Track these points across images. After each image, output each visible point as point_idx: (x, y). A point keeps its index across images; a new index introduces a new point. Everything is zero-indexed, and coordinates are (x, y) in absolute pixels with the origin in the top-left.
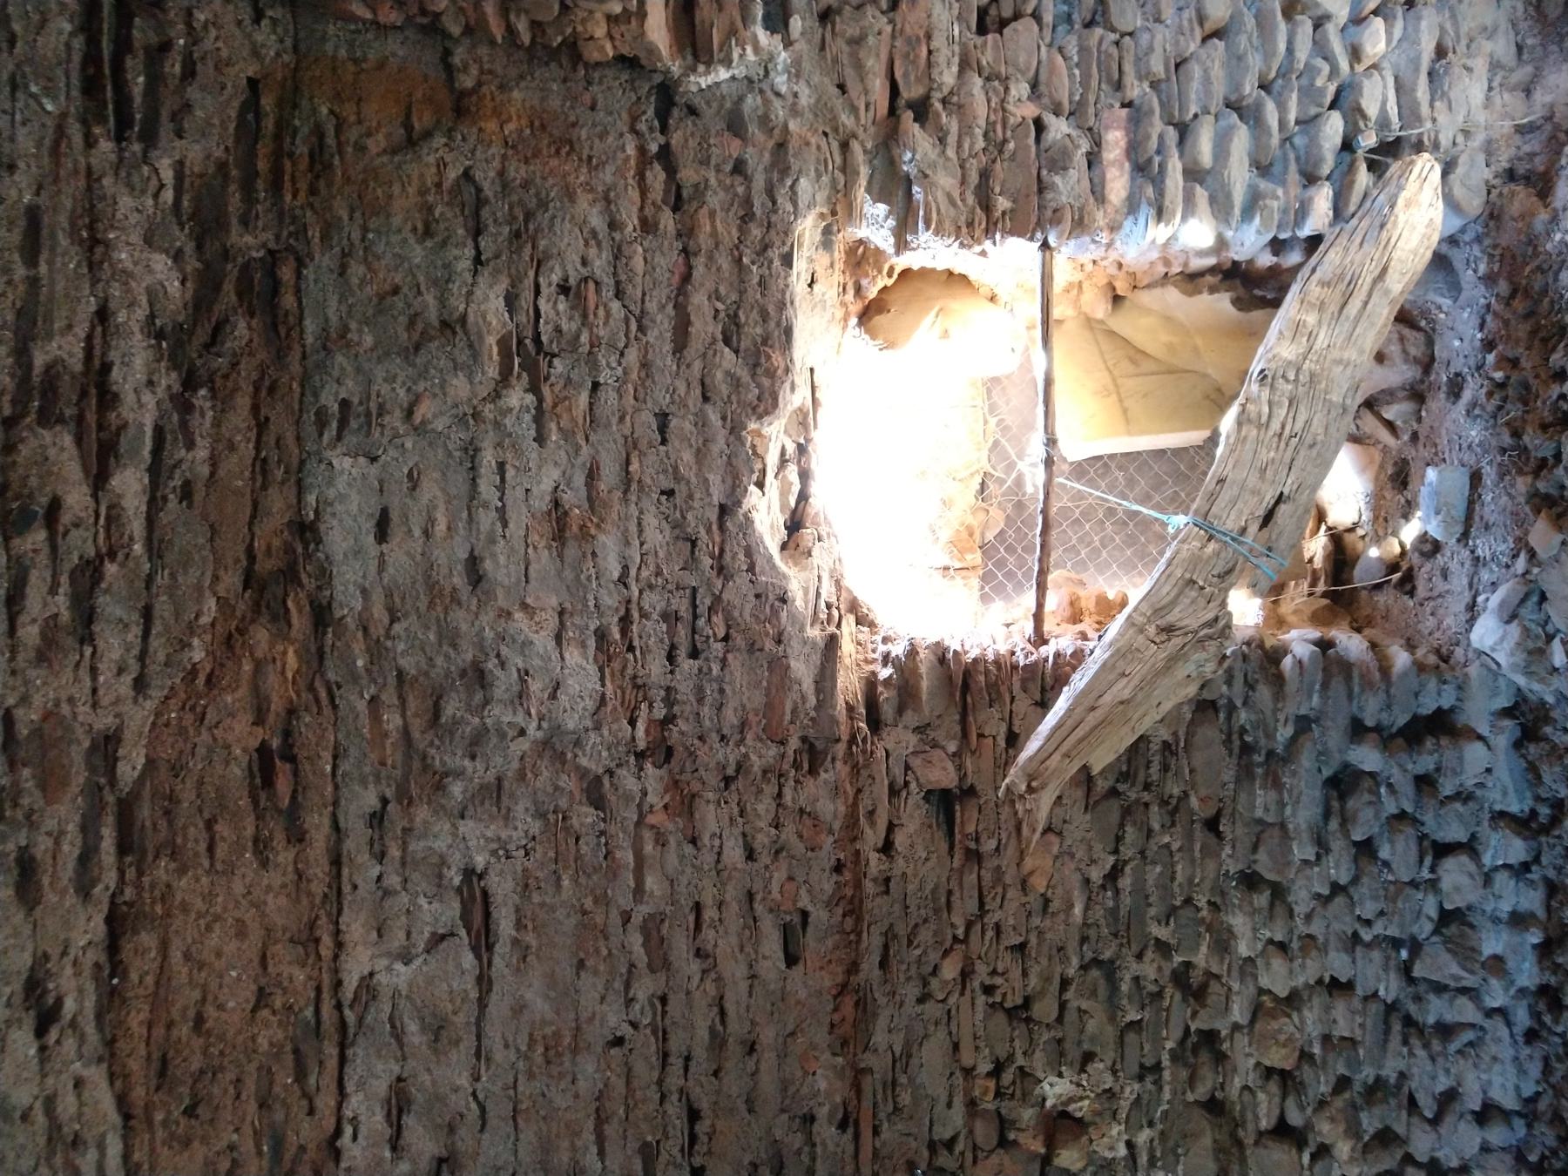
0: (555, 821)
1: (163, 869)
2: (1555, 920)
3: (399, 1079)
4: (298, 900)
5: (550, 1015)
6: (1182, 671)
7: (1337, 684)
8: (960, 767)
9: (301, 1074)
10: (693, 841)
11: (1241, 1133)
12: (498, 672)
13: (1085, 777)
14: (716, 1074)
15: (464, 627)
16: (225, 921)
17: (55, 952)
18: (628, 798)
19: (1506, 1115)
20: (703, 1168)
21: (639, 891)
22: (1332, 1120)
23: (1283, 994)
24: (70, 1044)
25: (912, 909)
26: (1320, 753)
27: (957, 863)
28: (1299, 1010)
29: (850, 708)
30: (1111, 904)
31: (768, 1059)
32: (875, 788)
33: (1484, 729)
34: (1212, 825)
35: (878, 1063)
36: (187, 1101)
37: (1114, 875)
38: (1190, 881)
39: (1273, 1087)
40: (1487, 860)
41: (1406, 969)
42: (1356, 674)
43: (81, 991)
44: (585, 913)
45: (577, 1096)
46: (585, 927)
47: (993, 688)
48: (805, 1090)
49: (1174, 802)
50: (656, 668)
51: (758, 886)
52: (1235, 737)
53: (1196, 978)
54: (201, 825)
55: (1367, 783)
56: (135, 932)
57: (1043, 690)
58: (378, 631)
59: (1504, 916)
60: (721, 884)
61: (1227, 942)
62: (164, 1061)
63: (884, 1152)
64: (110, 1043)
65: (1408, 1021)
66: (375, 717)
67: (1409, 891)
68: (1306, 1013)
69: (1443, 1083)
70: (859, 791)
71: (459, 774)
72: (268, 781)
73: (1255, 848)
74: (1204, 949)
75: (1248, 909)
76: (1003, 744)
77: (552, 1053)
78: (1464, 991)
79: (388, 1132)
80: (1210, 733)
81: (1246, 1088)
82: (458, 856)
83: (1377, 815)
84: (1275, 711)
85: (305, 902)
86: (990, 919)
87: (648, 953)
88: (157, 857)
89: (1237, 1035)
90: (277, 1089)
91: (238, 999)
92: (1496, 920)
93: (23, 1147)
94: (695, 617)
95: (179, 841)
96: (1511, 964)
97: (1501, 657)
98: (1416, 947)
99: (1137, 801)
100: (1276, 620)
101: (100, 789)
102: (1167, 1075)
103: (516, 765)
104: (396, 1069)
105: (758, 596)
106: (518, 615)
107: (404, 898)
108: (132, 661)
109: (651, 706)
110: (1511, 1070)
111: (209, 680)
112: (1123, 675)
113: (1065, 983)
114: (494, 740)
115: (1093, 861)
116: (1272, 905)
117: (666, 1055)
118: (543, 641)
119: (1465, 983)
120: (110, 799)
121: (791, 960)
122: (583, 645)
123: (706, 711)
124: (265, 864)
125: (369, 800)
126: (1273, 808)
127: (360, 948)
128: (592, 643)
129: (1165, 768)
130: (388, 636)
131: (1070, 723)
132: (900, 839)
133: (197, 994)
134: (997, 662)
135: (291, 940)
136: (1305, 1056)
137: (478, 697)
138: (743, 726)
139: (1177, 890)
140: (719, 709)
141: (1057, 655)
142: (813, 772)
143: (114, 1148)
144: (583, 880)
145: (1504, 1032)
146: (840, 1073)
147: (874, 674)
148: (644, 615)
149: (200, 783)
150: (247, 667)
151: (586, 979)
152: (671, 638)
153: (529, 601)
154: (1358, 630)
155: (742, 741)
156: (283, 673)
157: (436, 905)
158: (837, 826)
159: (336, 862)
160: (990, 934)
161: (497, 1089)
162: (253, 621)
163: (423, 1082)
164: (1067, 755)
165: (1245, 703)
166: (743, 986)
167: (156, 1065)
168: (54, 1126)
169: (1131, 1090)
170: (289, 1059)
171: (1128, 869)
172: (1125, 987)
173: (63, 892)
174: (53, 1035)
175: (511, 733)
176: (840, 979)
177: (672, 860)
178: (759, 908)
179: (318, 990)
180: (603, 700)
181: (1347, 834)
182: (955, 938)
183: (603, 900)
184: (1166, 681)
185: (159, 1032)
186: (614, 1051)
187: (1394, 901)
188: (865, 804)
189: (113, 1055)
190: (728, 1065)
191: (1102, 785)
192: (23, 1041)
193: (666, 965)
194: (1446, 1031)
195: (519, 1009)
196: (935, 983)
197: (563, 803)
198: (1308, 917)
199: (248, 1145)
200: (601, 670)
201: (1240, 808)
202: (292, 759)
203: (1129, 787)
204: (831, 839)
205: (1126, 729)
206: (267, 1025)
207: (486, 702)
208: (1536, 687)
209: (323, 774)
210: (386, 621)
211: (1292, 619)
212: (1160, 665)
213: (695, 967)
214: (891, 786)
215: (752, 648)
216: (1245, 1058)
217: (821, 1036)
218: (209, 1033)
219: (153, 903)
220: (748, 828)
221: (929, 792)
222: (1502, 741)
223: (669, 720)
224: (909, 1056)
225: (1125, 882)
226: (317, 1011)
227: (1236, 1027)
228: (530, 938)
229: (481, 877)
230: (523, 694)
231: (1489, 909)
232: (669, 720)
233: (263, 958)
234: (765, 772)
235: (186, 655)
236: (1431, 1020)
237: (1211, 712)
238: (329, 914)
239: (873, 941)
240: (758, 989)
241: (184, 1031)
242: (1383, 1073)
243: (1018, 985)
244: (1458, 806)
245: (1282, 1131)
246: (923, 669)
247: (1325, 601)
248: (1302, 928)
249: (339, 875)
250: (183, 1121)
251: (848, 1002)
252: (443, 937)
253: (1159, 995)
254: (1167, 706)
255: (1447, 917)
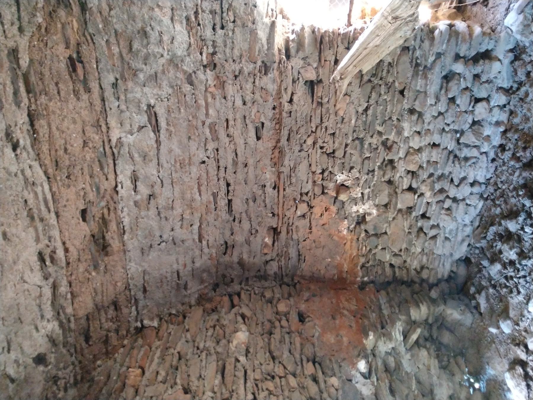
0: (177, 89)
1: (43, 99)
2: (510, 123)
3: (134, 171)
4: (92, 112)
5: (181, 154)
6: (398, 35)
7: (453, 40)
8: (317, 72)
9: (102, 168)
10: (225, 98)
11: (397, 190)
12: (151, 32)
13: (360, 75)
14: (235, 173)
15: (137, 13)
16: (69, 117)
17: (13, 125)
18: (201, 82)
19: (480, 184)
20: (231, 200)
21: (207, 114)
22: (426, 186)
23: (417, 148)
24: (25, 154)
25: (298, 122)
26: (443, 66)
27: (314, 106)
28: (421, 153)
29: (280, 50)
30: (364, 119)
31: (251, 169)
32: (287, 80)
33: (501, 57)
34: (402, 92)
35: (285, 170)
36: (66, 175)
37: (366, 110)
38: (392, 112)
39: (409, 176)
40: (492, 104)
41: (458, 140)
42: (460, 37)
43: (24, 138)
44: (189, 121)
45: (191, 178)
46: (189, 125)
47: (331, 42)
48: (263, 178)
49: (390, 84)
50: (208, 32)
51: (247, 114)
52: (414, 60)
53: (389, 143)
54: (54, 84)
55: (457, 77)
56: (38, 120)
57: (349, 43)
58: (105, 14)
59: (493, 122)
60: (235, 113)
61: (401, 132)
62: (57, 162)
63: (287, 196)
64: (38, 155)
65: (456, 156)
66: (109, 48)
67: (464, 114)
68: (423, 154)
69: (462, 175)
70: (282, 81)
71: (142, 70)
72: (75, 70)
73: (415, 100)
74: (393, 134)
75: (409, 120)
76: (333, 63)
77: (182, 165)
78: (475, 146)
79: (132, 186)
80: (406, 59)
81: (401, 177)
82: (144, 99)
83: (458, 88)
84: (429, 51)
85: (94, 113)
86: (324, 125)
87: (211, 135)
88: (40, 94)
89: (400, 161)
90: (95, 172)
91: (77, 144)
92: (490, 124)
93: (17, 184)
94: (222, 12)
95: (47, 89)
96: (492, 138)
97: (514, 29)
98: (462, 133)
99: (377, 84)
100: (436, 19)
101: (15, 69)
102: (376, 173)
103: (161, 68)
104: (133, 168)
105: (245, 4)
106: (156, 10)
107: (128, 114)
108: (16, 20)
109: (207, 48)
110: (485, 170)
111: (46, 29)
112: (378, 36)
113: (347, 145)
114: (152, 58)
115: (360, 105)
116: (418, 119)
117: (219, 167)
118: (166, 20)
119: (476, 144)
120: (20, 73)
121: (258, 138)
122: (181, 23)
123: (228, 51)
124: (78, 99)
125: (111, 79)
126: (423, 86)
127: (115, 129)
128: (184, 22)
129: (388, 72)
130: (109, 16)
131: (357, 54)
132: (295, 98)
133: (63, 142)
134: (333, 32)
135: (92, 125)
136: (421, 167)
137: (145, 42)
138: (241, 56)
139: (387, 114)
140: (232, 50)
141: (355, 29)
142: (266, 74)
143: (46, 187)
144: (188, 110)
145: (485, 159)
146: (274, 173)
147: (288, 37)
148: (203, 11)
149: (50, 69)
150: (59, 26)
151: (192, 143)
152: (214, 21)
153: (160, 4)
154: (465, 21)
155: (241, 61)
156: (73, 29)
157: (139, 116)
158: (274, 93)
159: (103, 100)
160: (324, 130)
161: (166, 175)
162: (58, 7)
163: (141, 174)
164: (355, 66)
165: (419, 48)
166: (243, 146)
167: (54, 163)
168: (26, 180)
169: (364, 177)
170: (97, 163)
171: (371, 108)
172: (366, 146)
173: (11, 104)
174: (18, 151)
175: (158, 56)
176: (274, 144)
177: (218, 104)
178: (248, 121)
179: (103, 142)
180: (190, 45)
181: (447, 95)
182: (312, 131)
183: (195, 117)
184: (393, 38)
185: (53, 152)
186: (202, 165)
187: (458, 117)
188: (284, 86)
189: (39, 159)
190: (238, 170)
191: (366, 78)
192: (8, 151)
193: (218, 139)
194: (466, 159)
195: (170, 151)
196: (304, 146)
197: (179, 83)
198: (429, 123)
199: (88, 188)
200: (189, 33)
201: (412, 86)
202: (82, 62)
203: (375, 79)
204: (272, 98)
205: (376, 57)
206: (88, 152)
207: (148, 44)
208: (524, 39)
209: (94, 68)
210: (108, 10)
211: (441, 17)
212: (391, 32)
213: (227, 140)
214: (293, 80)
215: (244, 26)
216: (401, 168)
217: (268, 162)
218: (69, 154)
219: (42, 111)
220: (243, 94)
221: (306, 82)
222: (506, 61)
223: (214, 53)
224: (295, 168)
225: (370, 112)
226: (104, 149)
227: (400, 158)
228: (172, 128)
229: (153, 107)
230: (161, 41)
231: (489, 120)
232: (214, 53)
233: (83, 131)
234: (249, 74)
235: (35, 19)
236: (463, 156)
237: (407, 51)
238: (103, 118)
239: (285, 133)
240: (247, 147)
241: (61, 152)
242: (445, 172)
243: (331, 146)
244: (486, 85)
245: (410, 189)
246: (306, 35)
247: (454, 10)
248: (426, 127)
249: (105, 105)
250: (67, 180)
251: (277, 151)
252: (143, 127)
253: (377, 149)
254: (392, 48)
255: (474, 123)
